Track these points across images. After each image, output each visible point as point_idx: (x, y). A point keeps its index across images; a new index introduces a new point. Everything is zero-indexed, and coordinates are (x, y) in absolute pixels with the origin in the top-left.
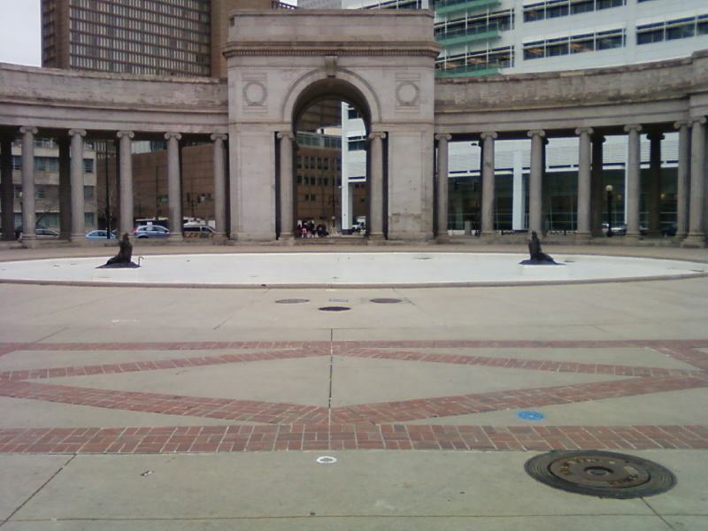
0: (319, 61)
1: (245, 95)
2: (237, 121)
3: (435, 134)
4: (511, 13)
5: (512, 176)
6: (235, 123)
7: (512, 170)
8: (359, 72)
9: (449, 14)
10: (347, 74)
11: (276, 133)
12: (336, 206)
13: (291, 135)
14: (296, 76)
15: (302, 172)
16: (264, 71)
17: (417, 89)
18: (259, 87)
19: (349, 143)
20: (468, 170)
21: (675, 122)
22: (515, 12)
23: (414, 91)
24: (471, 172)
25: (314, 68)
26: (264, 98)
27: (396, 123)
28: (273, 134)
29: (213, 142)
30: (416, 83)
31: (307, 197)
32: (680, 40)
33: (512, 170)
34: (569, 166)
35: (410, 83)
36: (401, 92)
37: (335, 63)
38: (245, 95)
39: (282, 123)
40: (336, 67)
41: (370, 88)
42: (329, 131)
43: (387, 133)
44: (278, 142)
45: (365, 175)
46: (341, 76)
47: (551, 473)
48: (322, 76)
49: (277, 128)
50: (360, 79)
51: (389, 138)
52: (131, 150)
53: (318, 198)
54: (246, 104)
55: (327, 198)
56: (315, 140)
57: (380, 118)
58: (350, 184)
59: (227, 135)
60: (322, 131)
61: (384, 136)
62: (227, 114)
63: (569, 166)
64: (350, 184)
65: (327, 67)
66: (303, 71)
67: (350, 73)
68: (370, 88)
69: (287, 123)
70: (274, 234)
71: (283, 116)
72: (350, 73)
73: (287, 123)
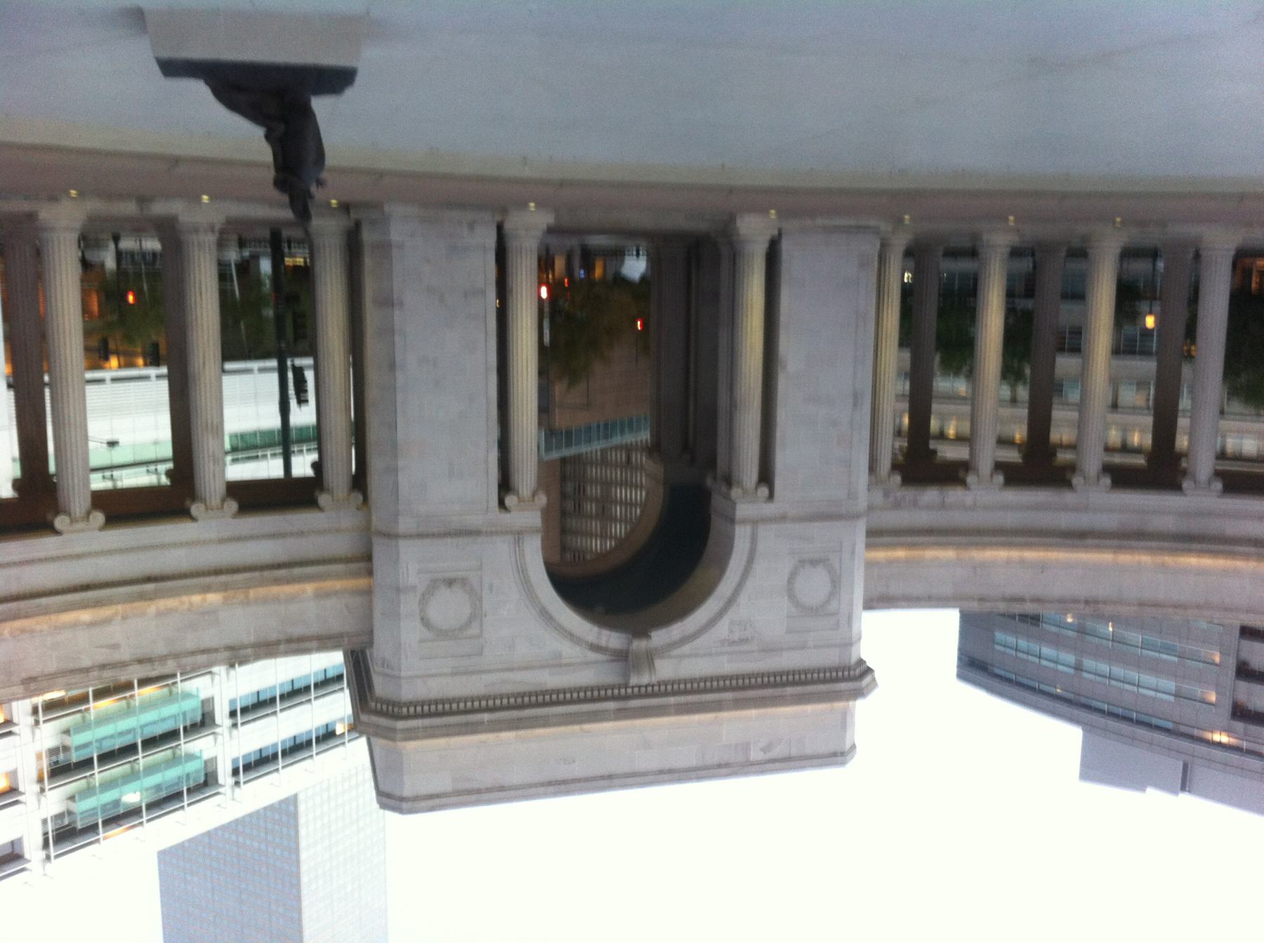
0: (665, 669)
4: (52, 851)
8: (570, 651)
9: (175, 760)
10: (603, 643)
11: (771, 496)
14: (722, 629)
15: (561, 420)
21: (102, 529)
22: (42, 854)
23: (434, 613)
24: (146, 378)
29: (1218, 474)
32: (82, 339)
36: (467, 610)
39: (755, 522)
40: (622, 657)
43: (502, 504)
44: (766, 476)
45: (167, 451)
46: (613, 639)
48: (659, 637)
49: (769, 509)
65: (649, 659)
66: (704, 641)
67: (595, 648)
69: (744, 522)
70: (786, 245)
72: (595, 648)
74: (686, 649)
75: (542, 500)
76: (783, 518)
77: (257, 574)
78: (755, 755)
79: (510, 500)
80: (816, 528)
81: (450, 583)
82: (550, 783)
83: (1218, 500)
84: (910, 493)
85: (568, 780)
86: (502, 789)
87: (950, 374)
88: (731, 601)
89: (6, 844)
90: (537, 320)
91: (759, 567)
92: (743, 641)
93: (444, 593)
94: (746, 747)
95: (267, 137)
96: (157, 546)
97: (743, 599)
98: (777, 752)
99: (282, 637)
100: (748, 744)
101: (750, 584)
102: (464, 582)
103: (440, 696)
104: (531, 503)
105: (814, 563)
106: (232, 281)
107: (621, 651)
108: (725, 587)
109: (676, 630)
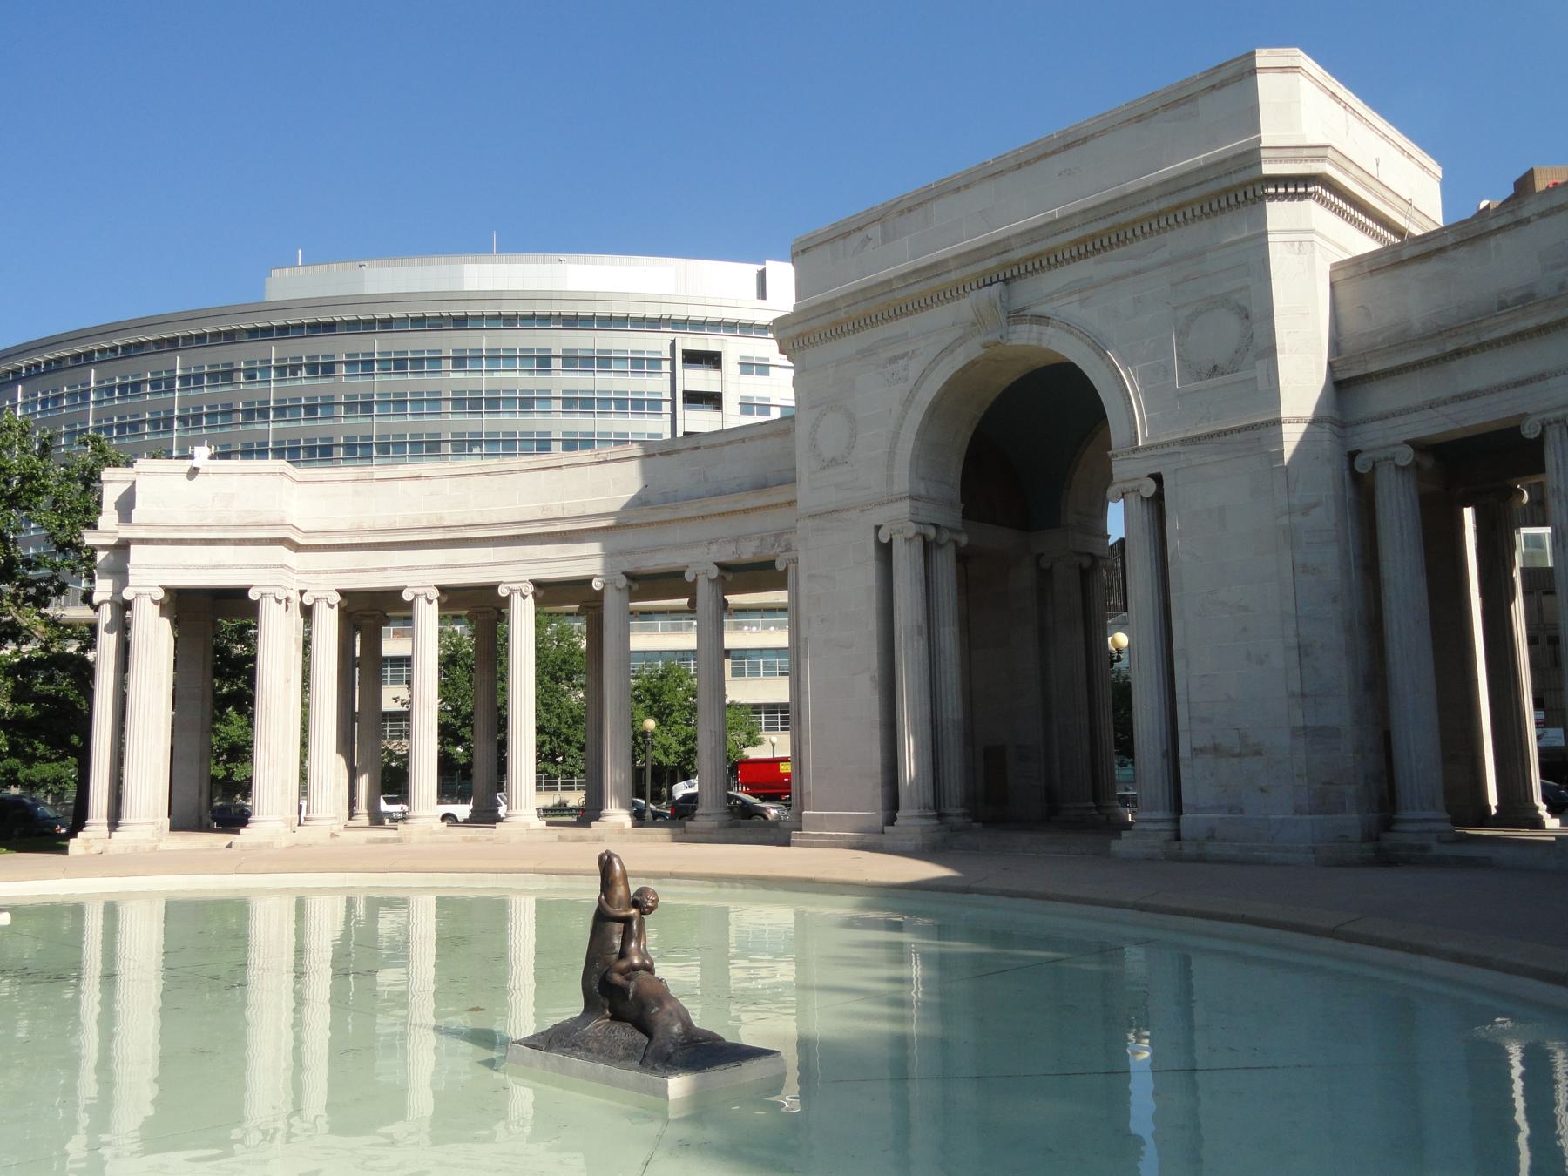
21: (1525, 416)
43: (1158, 478)
44: (885, 551)
72: (1041, 319)
77: (1486, 338)
78: (875, 231)
79: (1150, 488)
82: (1085, 140)
83: (1211, 380)
85: (1036, 162)
86: (1140, 118)
94: (886, 238)
95: (534, 974)
96: (1508, 388)
98: (856, 239)
99: (1451, 254)
100: (884, 242)
104: (1125, 491)
106: (1543, 752)
107: (1016, 323)
108: (916, 416)
109: (959, 360)
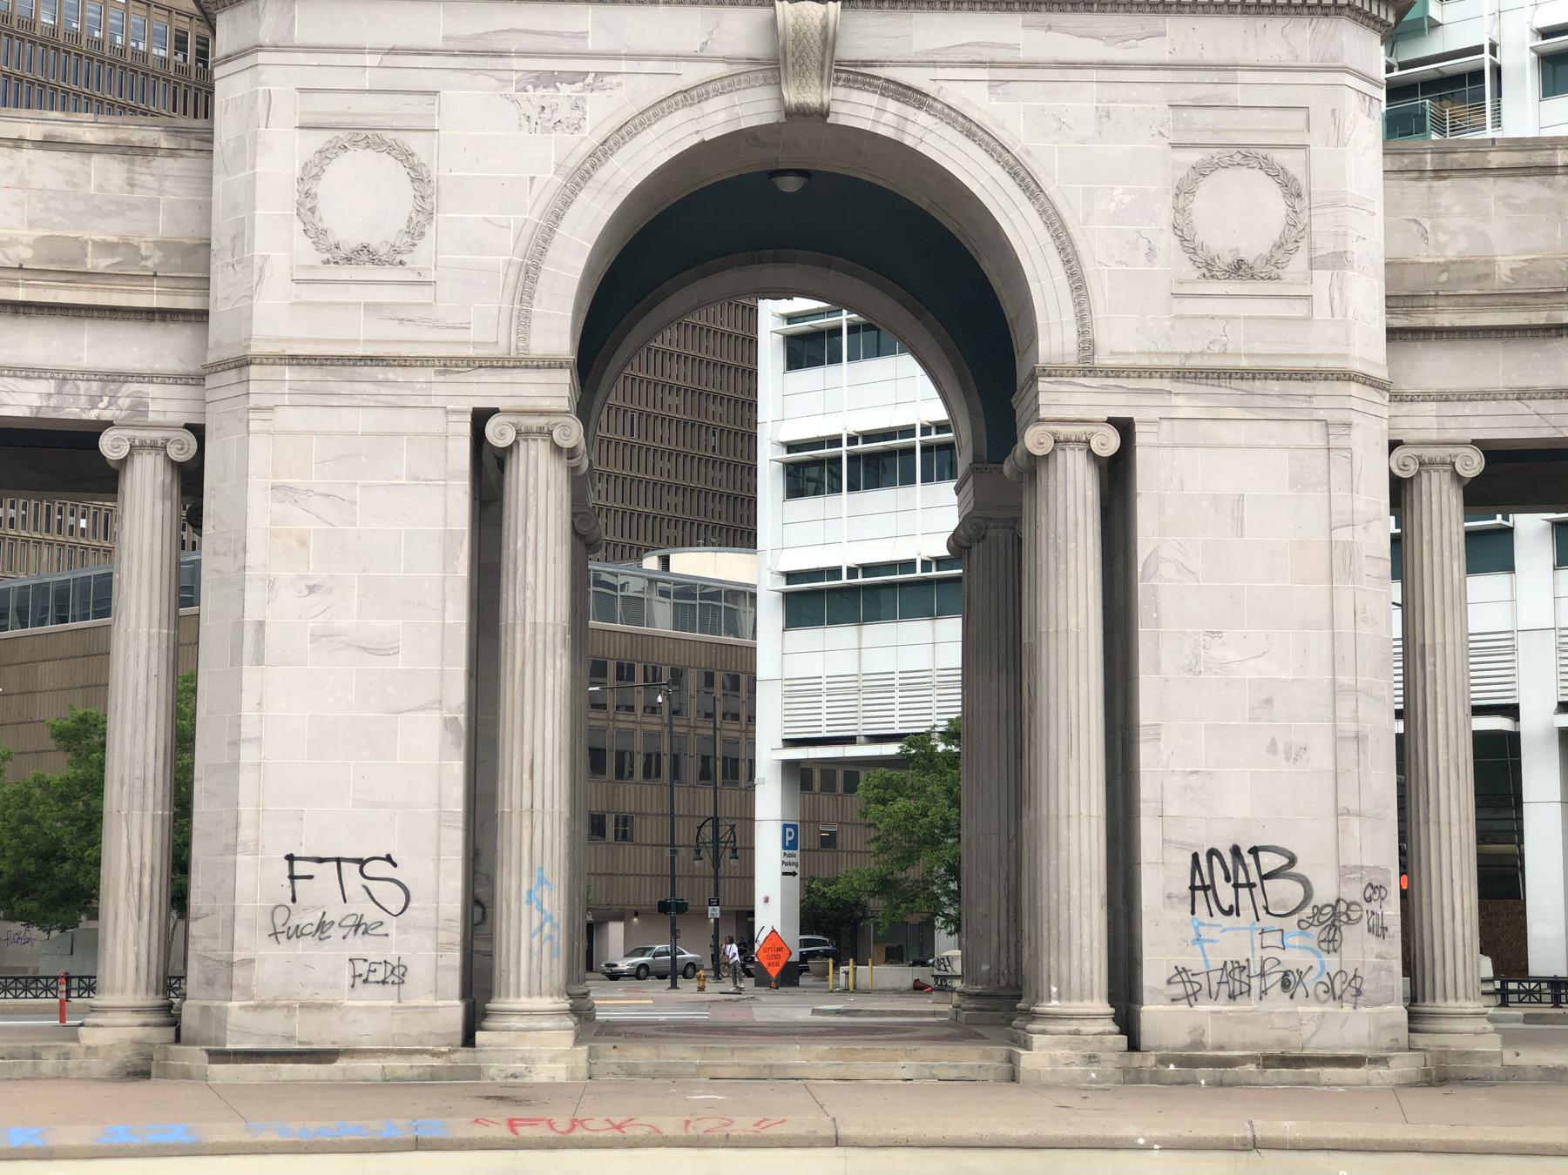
1: (307, 205)
2: (255, 350)
3: (1394, 445)
5: (1513, 739)
6: (243, 363)
7: (1512, 711)
11: (480, 418)
12: (729, 864)
13: (572, 433)
15: (656, 640)
16: (427, 80)
17: (1292, 190)
18: (388, 164)
19: (788, 597)
20: (861, 730)
23: (1274, 205)
25: (719, 69)
26: (415, 232)
27: (1179, 374)
28: (466, 428)
30: (1289, 161)
31: (624, 835)
33: (1512, 711)
34: (850, 740)
35: (1249, 156)
36: (1202, 205)
37: (828, 39)
38: (307, 205)
41: (1031, 187)
42: (693, 563)
43: (1125, 428)
47: (444, 601)
50: (971, 129)
51: (1142, 455)
52: (1479, 972)
53: (648, 830)
54: (306, 253)
55: (684, 833)
56: (636, 608)
57: (1087, 346)
58: (789, 767)
59: (198, 431)
60: (665, 561)
61: (1108, 443)
62: (200, 317)
63: (850, 740)
64: (789, 767)
66: (650, 86)
68: (1031, 187)
69: (551, 364)
70: (453, 1011)
71: (523, 320)
73: (551, 364)
74: (693, 74)
75: (1034, 440)
76: (448, 365)
80: (362, 336)
81: (1238, 269)
84: (76, 408)
87: (1154, 587)
88: (580, 176)
89: (782, 879)
90: (1142, 587)
91: (506, 252)
92: (546, 80)
93: (1253, 247)
97: (551, 181)
101: (533, 212)
102: (1209, 269)
103: (1260, 22)
105: (365, 254)
